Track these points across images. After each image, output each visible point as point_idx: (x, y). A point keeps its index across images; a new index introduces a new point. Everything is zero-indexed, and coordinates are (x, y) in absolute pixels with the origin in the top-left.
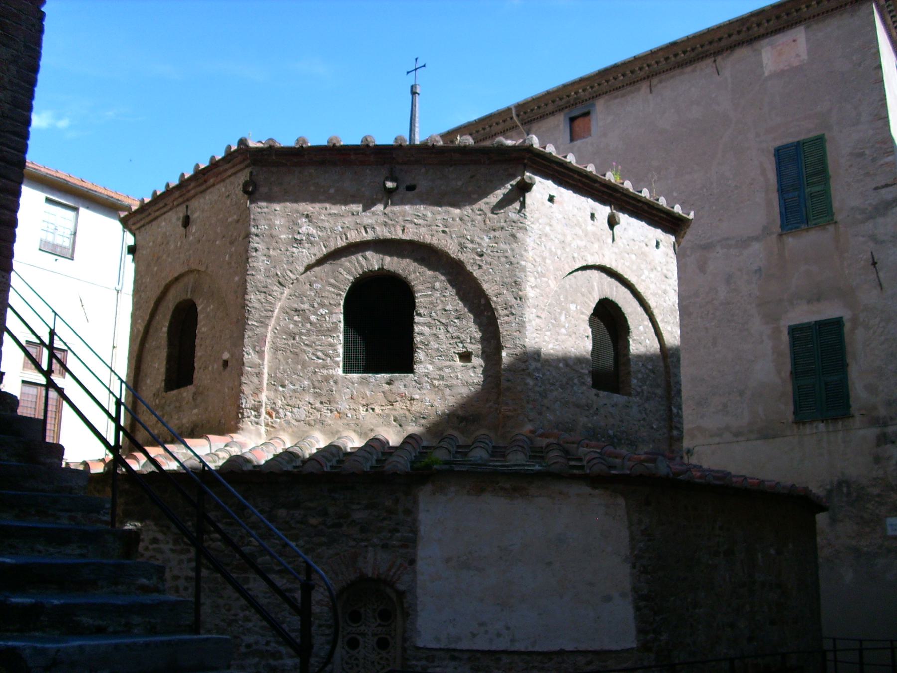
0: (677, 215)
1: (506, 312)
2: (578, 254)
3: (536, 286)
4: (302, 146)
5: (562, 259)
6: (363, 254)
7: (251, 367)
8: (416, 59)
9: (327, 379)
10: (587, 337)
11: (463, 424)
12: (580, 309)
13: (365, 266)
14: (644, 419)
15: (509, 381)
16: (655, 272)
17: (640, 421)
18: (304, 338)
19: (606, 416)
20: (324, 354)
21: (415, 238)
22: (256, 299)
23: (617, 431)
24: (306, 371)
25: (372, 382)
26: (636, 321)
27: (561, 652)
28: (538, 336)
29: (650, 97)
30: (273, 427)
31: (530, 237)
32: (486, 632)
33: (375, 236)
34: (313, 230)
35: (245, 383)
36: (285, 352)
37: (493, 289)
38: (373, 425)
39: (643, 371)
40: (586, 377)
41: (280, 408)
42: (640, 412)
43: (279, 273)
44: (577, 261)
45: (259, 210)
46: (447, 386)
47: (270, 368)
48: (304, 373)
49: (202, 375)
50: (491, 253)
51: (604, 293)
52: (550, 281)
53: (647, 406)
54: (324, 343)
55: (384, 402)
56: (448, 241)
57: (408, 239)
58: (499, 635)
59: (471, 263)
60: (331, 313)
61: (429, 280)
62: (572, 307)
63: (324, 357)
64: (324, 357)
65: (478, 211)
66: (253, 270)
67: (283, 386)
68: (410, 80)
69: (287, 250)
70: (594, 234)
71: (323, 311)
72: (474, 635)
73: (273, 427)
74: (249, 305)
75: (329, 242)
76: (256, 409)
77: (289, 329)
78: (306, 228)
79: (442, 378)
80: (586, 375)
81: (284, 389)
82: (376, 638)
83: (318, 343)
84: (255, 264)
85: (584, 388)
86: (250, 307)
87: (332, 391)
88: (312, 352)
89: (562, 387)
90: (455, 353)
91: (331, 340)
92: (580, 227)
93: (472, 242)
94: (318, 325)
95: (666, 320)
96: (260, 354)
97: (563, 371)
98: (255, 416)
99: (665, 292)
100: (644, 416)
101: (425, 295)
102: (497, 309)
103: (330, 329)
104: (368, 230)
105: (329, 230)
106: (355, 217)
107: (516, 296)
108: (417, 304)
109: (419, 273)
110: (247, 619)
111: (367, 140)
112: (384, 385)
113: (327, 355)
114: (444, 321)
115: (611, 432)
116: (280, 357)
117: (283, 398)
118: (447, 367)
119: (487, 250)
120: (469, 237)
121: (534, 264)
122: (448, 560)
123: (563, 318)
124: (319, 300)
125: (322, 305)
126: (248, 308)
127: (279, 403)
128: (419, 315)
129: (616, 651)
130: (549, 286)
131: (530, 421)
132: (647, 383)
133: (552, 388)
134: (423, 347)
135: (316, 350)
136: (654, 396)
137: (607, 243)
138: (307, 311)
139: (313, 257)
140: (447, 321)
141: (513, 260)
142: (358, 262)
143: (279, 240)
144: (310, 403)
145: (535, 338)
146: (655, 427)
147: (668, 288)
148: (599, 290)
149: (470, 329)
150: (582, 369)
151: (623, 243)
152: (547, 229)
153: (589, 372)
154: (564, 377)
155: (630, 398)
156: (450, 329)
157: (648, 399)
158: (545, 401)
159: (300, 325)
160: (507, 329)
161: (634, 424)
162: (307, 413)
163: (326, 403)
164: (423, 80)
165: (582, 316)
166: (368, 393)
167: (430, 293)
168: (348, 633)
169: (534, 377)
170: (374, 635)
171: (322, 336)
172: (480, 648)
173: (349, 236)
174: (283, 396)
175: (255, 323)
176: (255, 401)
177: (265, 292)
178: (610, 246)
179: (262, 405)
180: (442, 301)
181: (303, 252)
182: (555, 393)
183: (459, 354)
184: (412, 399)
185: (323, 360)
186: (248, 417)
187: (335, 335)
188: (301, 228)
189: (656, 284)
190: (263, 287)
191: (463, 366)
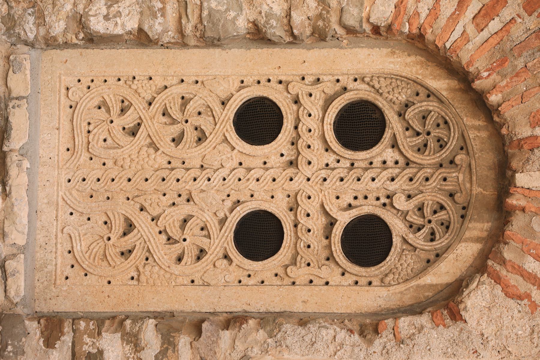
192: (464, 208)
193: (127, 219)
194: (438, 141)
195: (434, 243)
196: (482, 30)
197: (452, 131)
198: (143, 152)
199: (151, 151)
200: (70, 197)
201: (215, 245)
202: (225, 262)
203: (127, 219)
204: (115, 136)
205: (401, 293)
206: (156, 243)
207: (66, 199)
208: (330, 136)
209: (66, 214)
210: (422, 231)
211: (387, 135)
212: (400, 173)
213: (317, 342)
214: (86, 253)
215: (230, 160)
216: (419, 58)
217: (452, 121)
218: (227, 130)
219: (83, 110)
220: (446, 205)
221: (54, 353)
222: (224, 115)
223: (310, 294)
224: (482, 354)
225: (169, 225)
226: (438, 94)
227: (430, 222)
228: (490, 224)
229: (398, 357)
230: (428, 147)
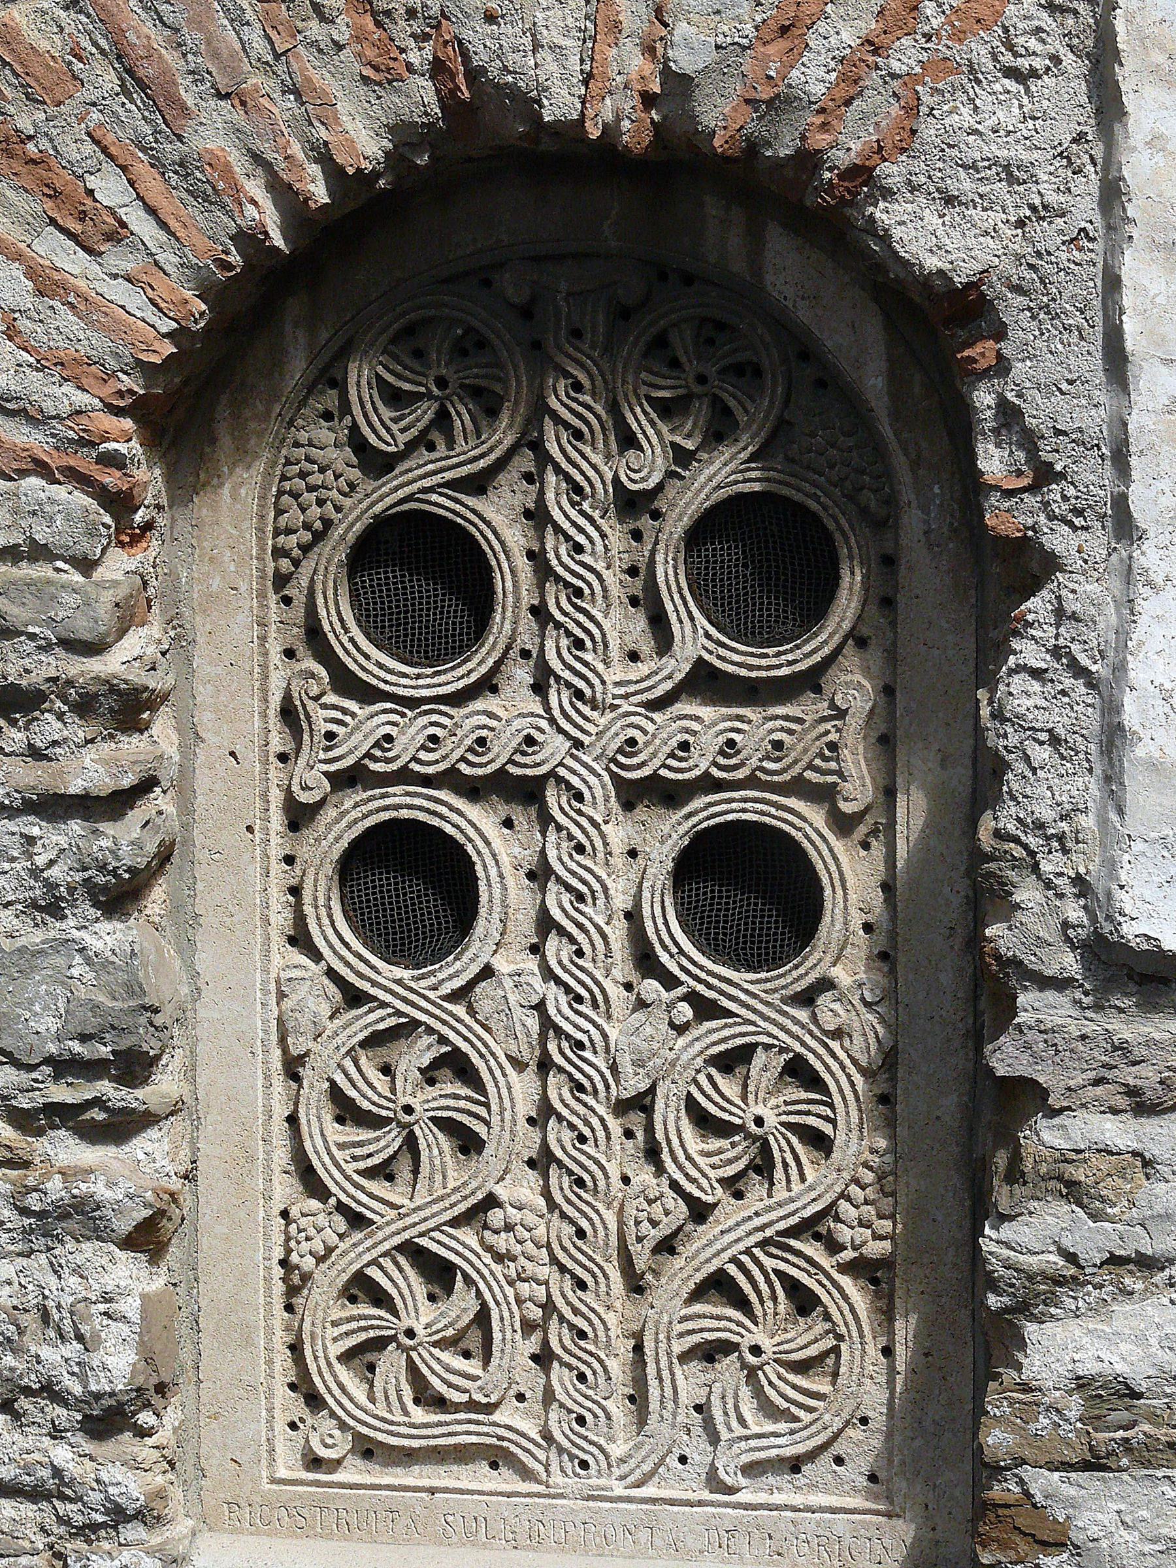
192: (663, 276)
193: (698, 1294)
194: (464, 353)
195: (766, 363)
196: (123, 225)
197: (433, 312)
198: (502, 1242)
199: (496, 1217)
200: (632, 1463)
201: (775, 1031)
202: (824, 1000)
203: (698, 1294)
204: (451, 1324)
205: (915, 465)
206: (769, 1209)
207: (637, 1474)
208: (452, 680)
209: (685, 1475)
210: (732, 403)
211: (442, 504)
212: (558, 470)
213: (1050, 725)
214: (797, 1419)
215: (522, 979)
216: (223, 412)
217: (404, 314)
218: (435, 989)
219: (376, 1417)
220: (653, 331)
221: (1080, 1524)
222: (388, 998)
223: (920, 745)
224: (1083, 224)
225: (714, 1167)
226: (326, 356)
227: (702, 379)
228: (707, 199)
229: (1092, 477)
230: (484, 383)
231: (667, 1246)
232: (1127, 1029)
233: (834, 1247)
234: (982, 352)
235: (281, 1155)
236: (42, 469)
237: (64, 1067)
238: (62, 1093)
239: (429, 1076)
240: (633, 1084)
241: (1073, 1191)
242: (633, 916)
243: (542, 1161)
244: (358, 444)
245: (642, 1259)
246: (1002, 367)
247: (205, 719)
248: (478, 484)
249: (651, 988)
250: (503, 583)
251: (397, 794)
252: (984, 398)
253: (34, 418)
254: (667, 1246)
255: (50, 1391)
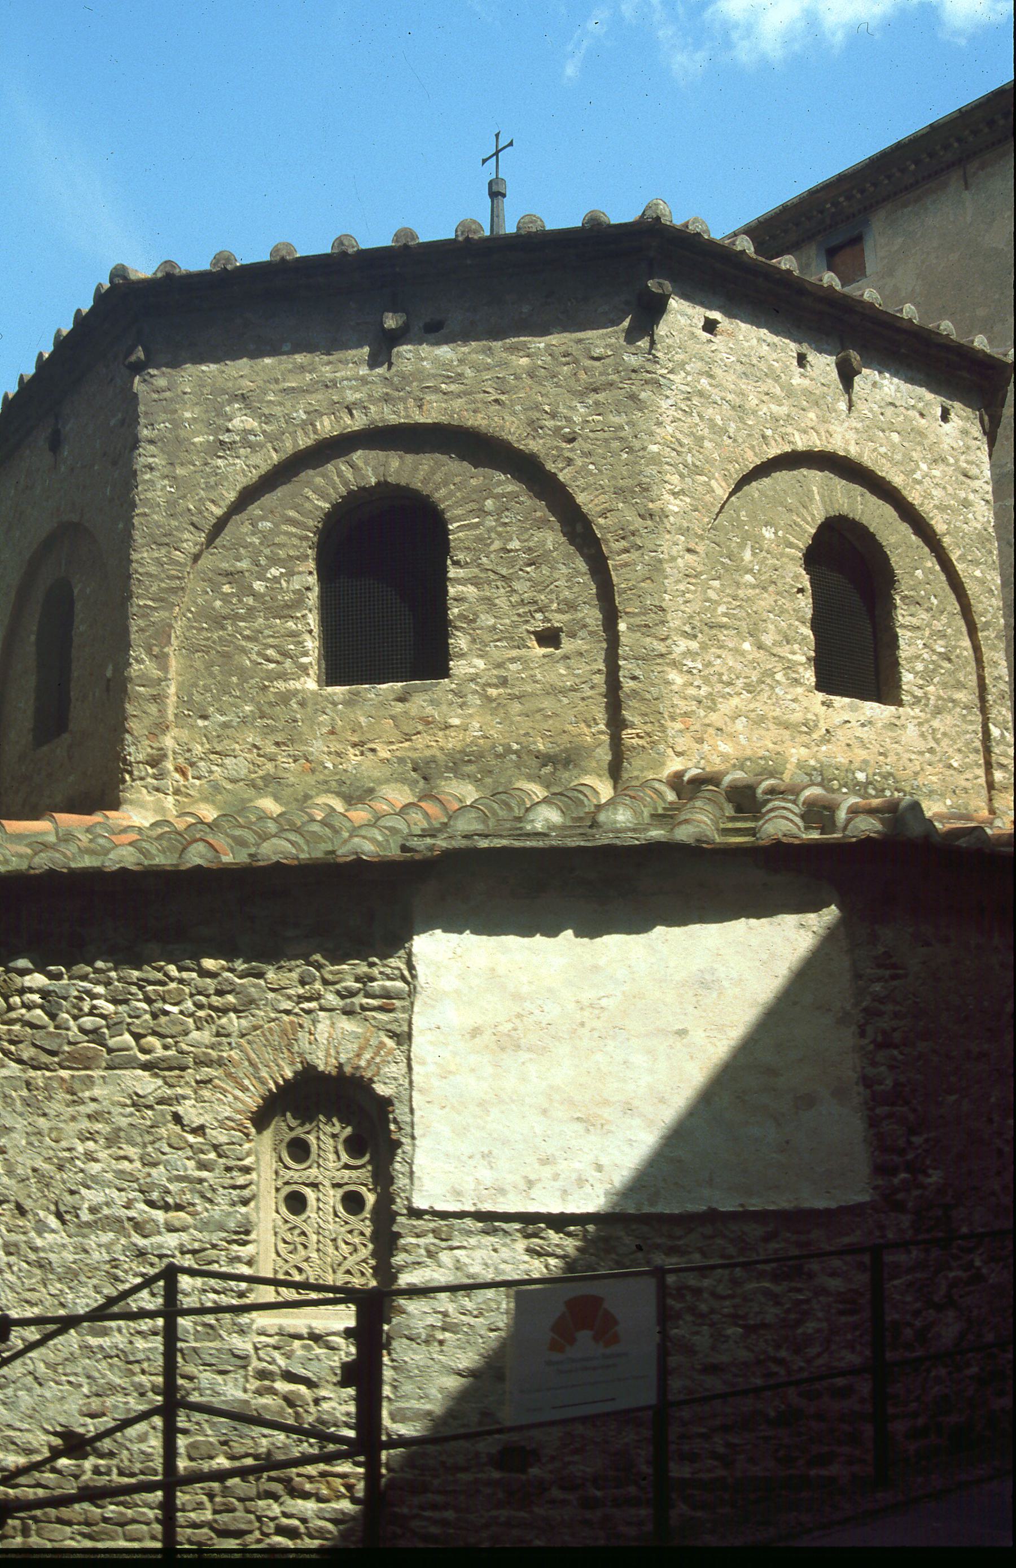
0: (980, 355)
1: (623, 544)
2: (774, 430)
3: (682, 492)
4: (225, 268)
5: (740, 440)
6: (347, 458)
7: (143, 686)
8: (497, 135)
9: (285, 698)
10: (801, 591)
11: (549, 769)
12: (784, 537)
13: (352, 480)
14: (931, 751)
15: (634, 678)
16: (942, 467)
17: (922, 753)
18: (242, 624)
19: (848, 745)
20: (279, 652)
21: (444, 419)
22: (152, 559)
23: (874, 774)
24: (245, 685)
25: (371, 700)
26: (908, 560)
27: (712, 1216)
28: (692, 588)
29: (966, 195)
30: (188, 795)
31: (667, 397)
32: (556, 1177)
33: (368, 423)
34: (252, 423)
35: (135, 716)
36: (207, 653)
37: (596, 501)
38: (373, 781)
39: (926, 656)
40: (801, 669)
41: (201, 759)
42: (922, 735)
43: (192, 507)
44: (773, 443)
45: (155, 396)
46: (513, 697)
47: (180, 687)
48: (242, 690)
49: (80, 715)
50: (591, 434)
51: (837, 506)
52: (713, 483)
53: (936, 723)
54: (278, 632)
55: (395, 735)
56: (506, 418)
57: (430, 421)
58: (581, 1182)
59: (554, 456)
60: (291, 574)
61: (474, 496)
62: (768, 533)
63: (279, 658)
64: (279, 658)
65: (564, 356)
66: (145, 506)
67: (205, 717)
68: (488, 173)
69: (206, 464)
70: (807, 393)
71: (274, 572)
72: (530, 1183)
73: (188, 795)
74: (140, 570)
75: (283, 441)
76: (154, 762)
77: (214, 609)
78: (242, 421)
79: (504, 682)
80: (802, 664)
81: (206, 723)
82: (340, 1192)
83: (267, 632)
84: (149, 495)
85: (800, 690)
86: (141, 575)
87: (295, 721)
88: (256, 649)
89: (749, 688)
90: (528, 631)
91: (290, 624)
92: (777, 379)
93: (553, 416)
94: (267, 598)
95: (970, 558)
96: (161, 660)
97: (750, 657)
98: (155, 777)
99: (966, 504)
100: (933, 744)
101: (468, 525)
102: (607, 541)
103: (289, 603)
104: (354, 412)
105: (282, 420)
106: (330, 391)
107: (642, 512)
108: (452, 544)
109: (454, 484)
110: (90, 1157)
111: (341, 243)
112: (393, 703)
113: (285, 654)
114: (504, 572)
115: (861, 776)
116: (198, 664)
117: (204, 740)
118: (513, 660)
119: (582, 429)
120: (547, 408)
121: (679, 449)
122: (475, 1032)
123: (747, 555)
124: (267, 551)
125: (274, 561)
126: (138, 576)
127: (198, 749)
128: (456, 563)
129: (828, 1212)
130: (713, 491)
131: (679, 754)
132: (935, 680)
133: (727, 690)
134: (465, 625)
135: (264, 644)
136: (950, 705)
137: (835, 411)
138: (247, 574)
139: (254, 471)
140: (511, 571)
141: (637, 444)
142: (340, 474)
143: (192, 447)
144: (255, 746)
145: (684, 593)
146: (955, 764)
147: (971, 497)
148: (824, 502)
149: (556, 584)
150: (794, 653)
151: (871, 410)
152: (704, 381)
153: (808, 659)
154: (755, 668)
155: (901, 709)
156: (516, 585)
157: (938, 711)
158: (714, 717)
159: (234, 600)
160: (627, 576)
161: (910, 760)
162: (251, 766)
163: (284, 744)
164: (509, 167)
165: (788, 550)
166: (363, 720)
167: (477, 520)
168: (287, 1183)
169: (685, 668)
170: (336, 1186)
171: (274, 617)
172: (543, 1210)
173: (319, 427)
174: (205, 736)
175: (150, 603)
176: (152, 748)
177: (167, 544)
178: (843, 416)
179: (165, 756)
180: (499, 534)
181: (234, 464)
182: (735, 701)
183: (534, 633)
184: (448, 727)
185: (278, 662)
186: (142, 779)
187: (299, 615)
188: (230, 420)
189: (944, 488)
190: (165, 535)
191: (544, 656)
231: (339, 1265)
232: (415, 1223)
233: (367, 1264)
234: (390, 1109)
235: (273, 1250)
236: (234, 1129)
237: (236, 1233)
238: (235, 1237)
239: (299, 1235)
240: (334, 1236)
241: (406, 1251)
242: (334, 1207)
243: (318, 1250)
244: (288, 1126)
245: (335, 1267)
246: (393, 1112)
247: (262, 1174)
248: (308, 1133)
249: (337, 1219)
250: (312, 1150)
251: (294, 1186)
252: (391, 1116)
253: (233, 1121)
254: (339, 1265)
255: (232, 1290)
